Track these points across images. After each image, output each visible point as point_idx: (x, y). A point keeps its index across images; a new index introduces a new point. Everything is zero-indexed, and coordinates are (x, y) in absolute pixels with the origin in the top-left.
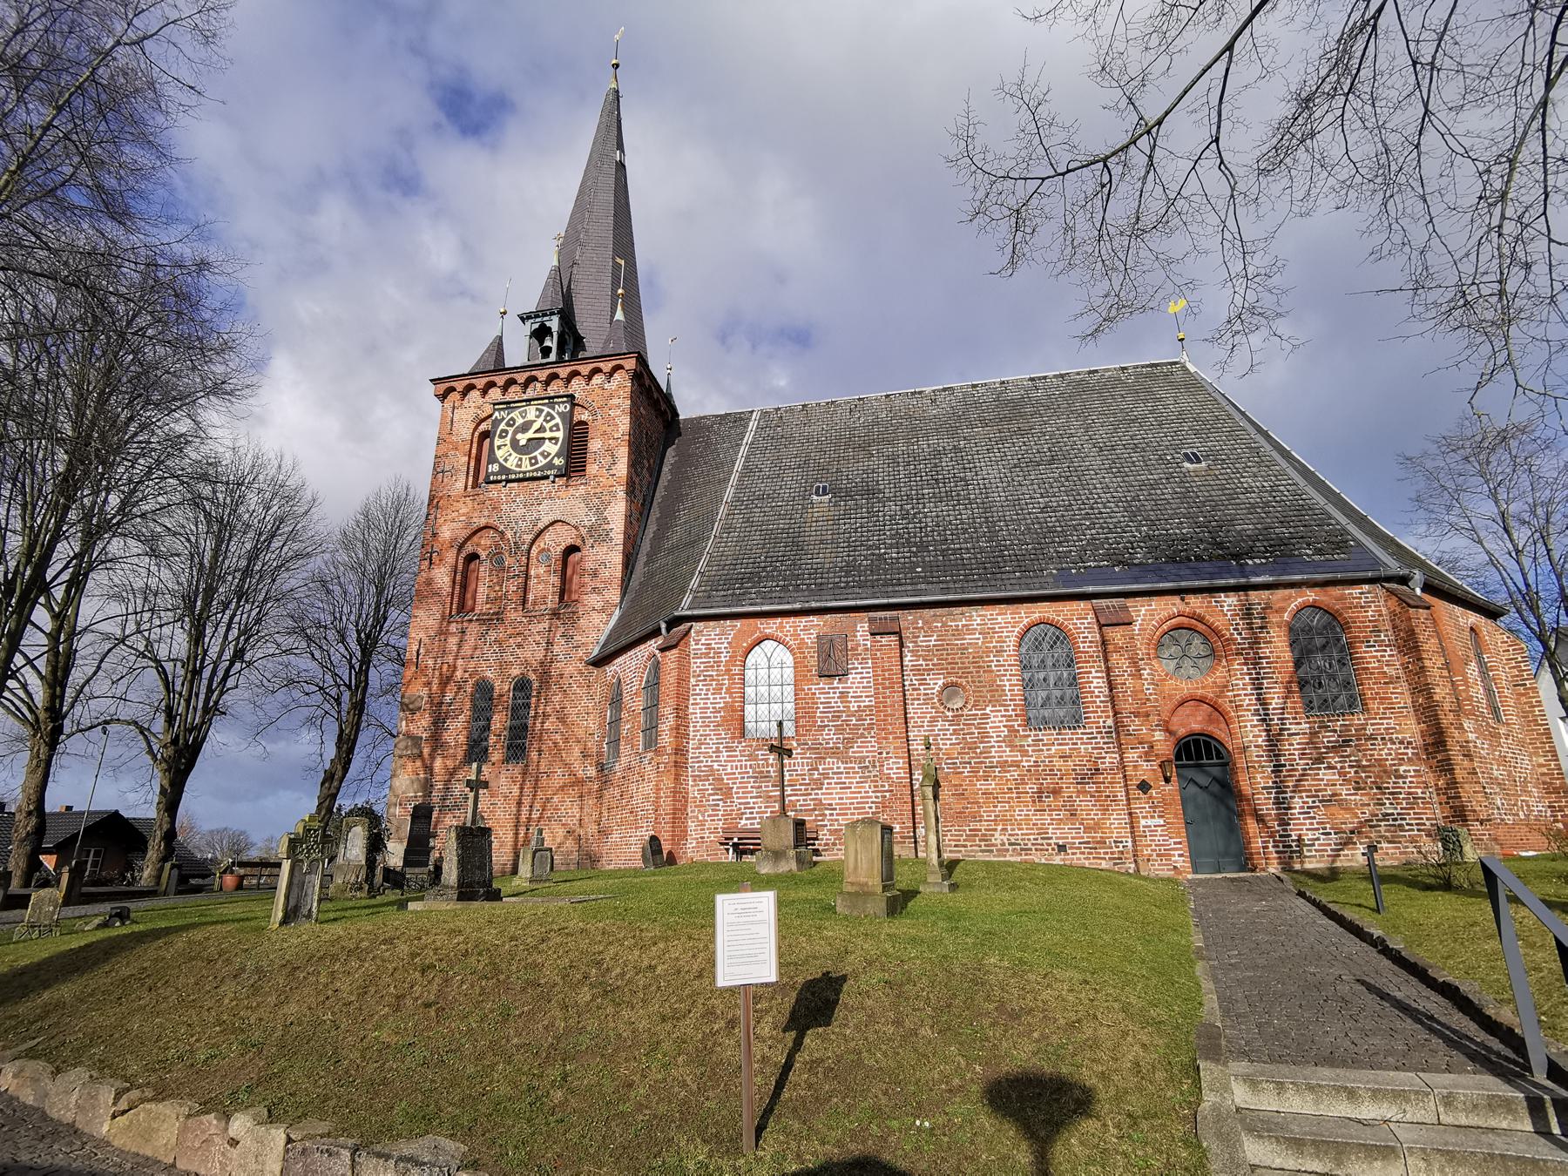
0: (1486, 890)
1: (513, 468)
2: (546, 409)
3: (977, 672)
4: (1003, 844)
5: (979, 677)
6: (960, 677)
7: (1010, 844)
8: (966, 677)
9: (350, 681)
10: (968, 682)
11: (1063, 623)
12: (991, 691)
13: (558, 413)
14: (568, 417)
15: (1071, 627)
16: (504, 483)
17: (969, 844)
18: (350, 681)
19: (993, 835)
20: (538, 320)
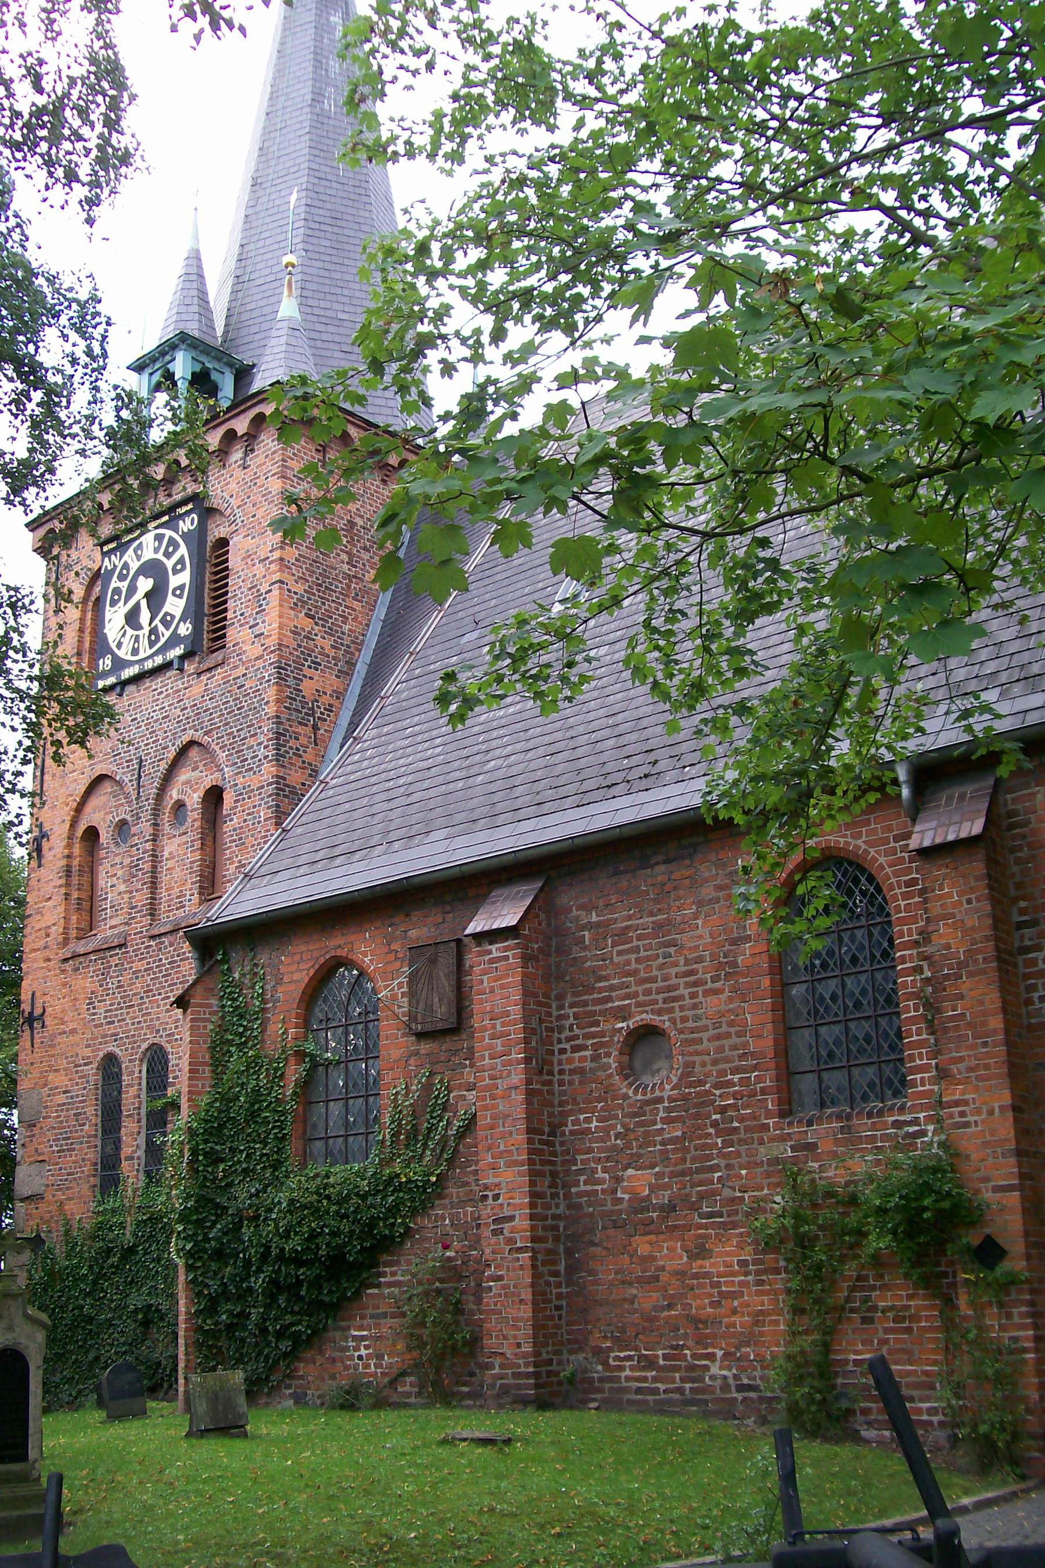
0: (893, 1367)
1: (129, 657)
2: (168, 533)
3: (693, 996)
4: (725, 1388)
5: (695, 1007)
6: (660, 1012)
7: (741, 1388)
8: (671, 1010)
9: (870, 127)
10: (673, 1021)
11: (866, 852)
12: (718, 1037)
13: (184, 536)
14: (197, 540)
15: (882, 860)
16: (118, 689)
17: (662, 1387)
18: (870, 127)
19: (706, 1368)
20: (158, 365)
